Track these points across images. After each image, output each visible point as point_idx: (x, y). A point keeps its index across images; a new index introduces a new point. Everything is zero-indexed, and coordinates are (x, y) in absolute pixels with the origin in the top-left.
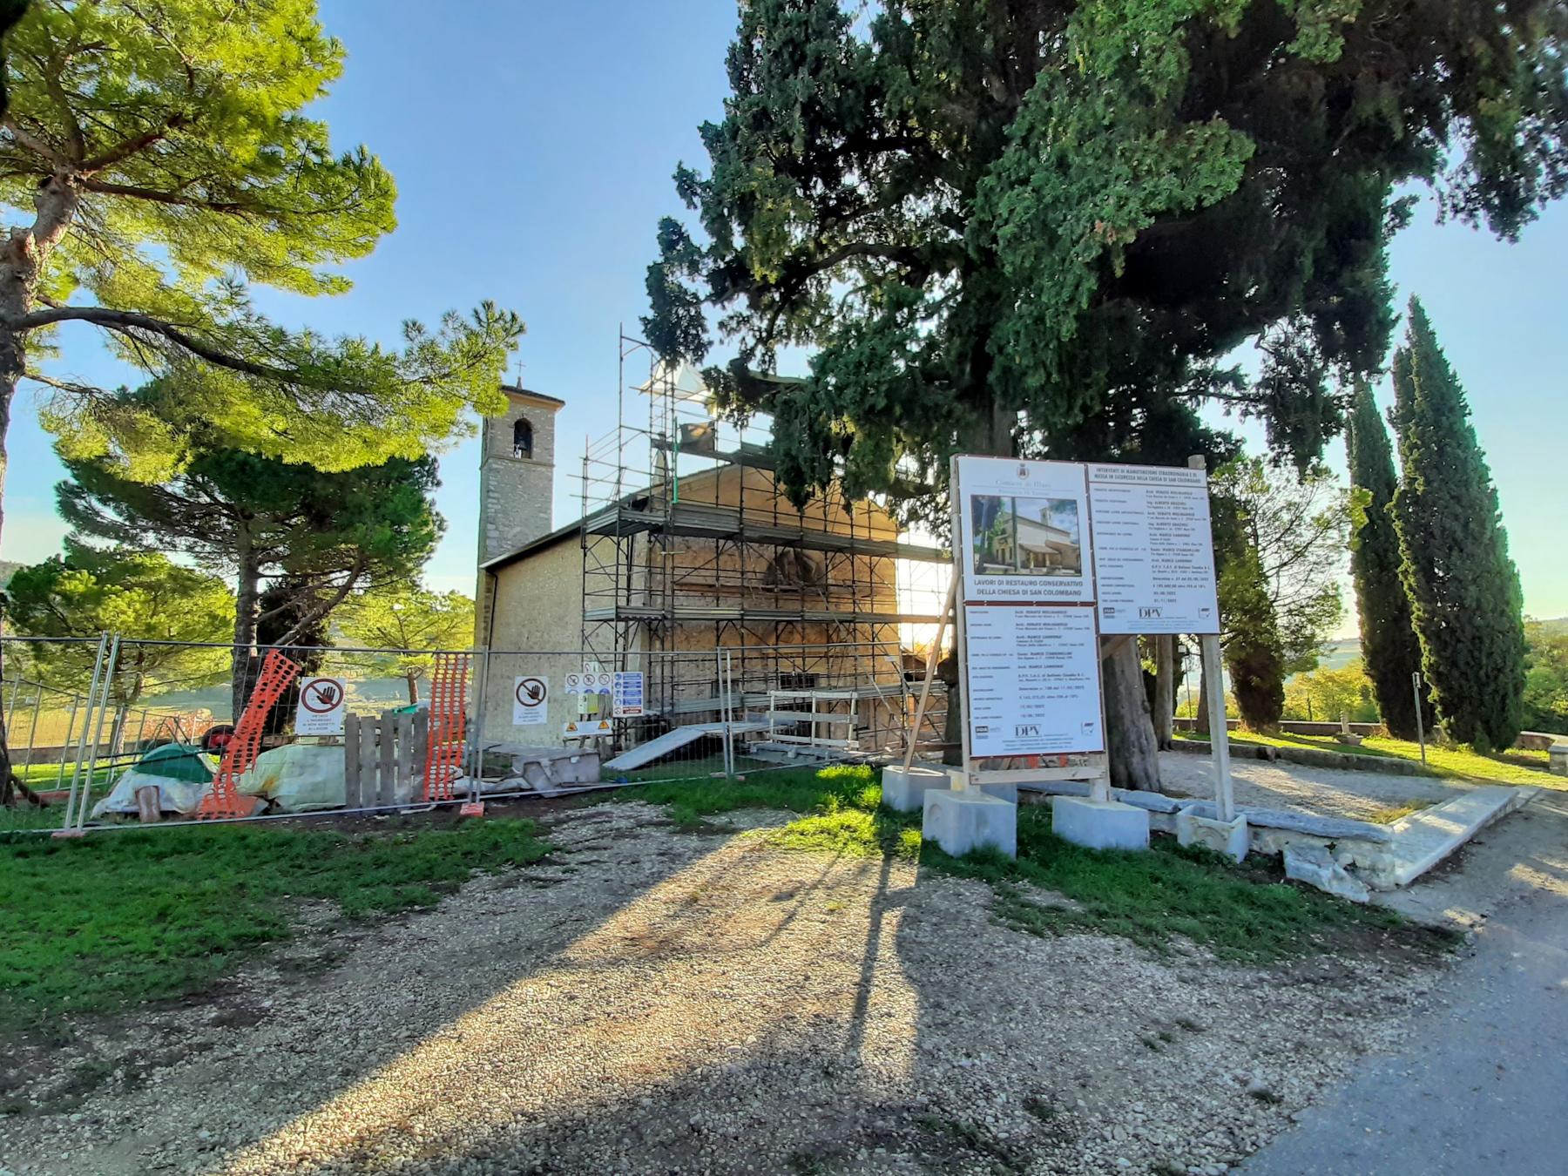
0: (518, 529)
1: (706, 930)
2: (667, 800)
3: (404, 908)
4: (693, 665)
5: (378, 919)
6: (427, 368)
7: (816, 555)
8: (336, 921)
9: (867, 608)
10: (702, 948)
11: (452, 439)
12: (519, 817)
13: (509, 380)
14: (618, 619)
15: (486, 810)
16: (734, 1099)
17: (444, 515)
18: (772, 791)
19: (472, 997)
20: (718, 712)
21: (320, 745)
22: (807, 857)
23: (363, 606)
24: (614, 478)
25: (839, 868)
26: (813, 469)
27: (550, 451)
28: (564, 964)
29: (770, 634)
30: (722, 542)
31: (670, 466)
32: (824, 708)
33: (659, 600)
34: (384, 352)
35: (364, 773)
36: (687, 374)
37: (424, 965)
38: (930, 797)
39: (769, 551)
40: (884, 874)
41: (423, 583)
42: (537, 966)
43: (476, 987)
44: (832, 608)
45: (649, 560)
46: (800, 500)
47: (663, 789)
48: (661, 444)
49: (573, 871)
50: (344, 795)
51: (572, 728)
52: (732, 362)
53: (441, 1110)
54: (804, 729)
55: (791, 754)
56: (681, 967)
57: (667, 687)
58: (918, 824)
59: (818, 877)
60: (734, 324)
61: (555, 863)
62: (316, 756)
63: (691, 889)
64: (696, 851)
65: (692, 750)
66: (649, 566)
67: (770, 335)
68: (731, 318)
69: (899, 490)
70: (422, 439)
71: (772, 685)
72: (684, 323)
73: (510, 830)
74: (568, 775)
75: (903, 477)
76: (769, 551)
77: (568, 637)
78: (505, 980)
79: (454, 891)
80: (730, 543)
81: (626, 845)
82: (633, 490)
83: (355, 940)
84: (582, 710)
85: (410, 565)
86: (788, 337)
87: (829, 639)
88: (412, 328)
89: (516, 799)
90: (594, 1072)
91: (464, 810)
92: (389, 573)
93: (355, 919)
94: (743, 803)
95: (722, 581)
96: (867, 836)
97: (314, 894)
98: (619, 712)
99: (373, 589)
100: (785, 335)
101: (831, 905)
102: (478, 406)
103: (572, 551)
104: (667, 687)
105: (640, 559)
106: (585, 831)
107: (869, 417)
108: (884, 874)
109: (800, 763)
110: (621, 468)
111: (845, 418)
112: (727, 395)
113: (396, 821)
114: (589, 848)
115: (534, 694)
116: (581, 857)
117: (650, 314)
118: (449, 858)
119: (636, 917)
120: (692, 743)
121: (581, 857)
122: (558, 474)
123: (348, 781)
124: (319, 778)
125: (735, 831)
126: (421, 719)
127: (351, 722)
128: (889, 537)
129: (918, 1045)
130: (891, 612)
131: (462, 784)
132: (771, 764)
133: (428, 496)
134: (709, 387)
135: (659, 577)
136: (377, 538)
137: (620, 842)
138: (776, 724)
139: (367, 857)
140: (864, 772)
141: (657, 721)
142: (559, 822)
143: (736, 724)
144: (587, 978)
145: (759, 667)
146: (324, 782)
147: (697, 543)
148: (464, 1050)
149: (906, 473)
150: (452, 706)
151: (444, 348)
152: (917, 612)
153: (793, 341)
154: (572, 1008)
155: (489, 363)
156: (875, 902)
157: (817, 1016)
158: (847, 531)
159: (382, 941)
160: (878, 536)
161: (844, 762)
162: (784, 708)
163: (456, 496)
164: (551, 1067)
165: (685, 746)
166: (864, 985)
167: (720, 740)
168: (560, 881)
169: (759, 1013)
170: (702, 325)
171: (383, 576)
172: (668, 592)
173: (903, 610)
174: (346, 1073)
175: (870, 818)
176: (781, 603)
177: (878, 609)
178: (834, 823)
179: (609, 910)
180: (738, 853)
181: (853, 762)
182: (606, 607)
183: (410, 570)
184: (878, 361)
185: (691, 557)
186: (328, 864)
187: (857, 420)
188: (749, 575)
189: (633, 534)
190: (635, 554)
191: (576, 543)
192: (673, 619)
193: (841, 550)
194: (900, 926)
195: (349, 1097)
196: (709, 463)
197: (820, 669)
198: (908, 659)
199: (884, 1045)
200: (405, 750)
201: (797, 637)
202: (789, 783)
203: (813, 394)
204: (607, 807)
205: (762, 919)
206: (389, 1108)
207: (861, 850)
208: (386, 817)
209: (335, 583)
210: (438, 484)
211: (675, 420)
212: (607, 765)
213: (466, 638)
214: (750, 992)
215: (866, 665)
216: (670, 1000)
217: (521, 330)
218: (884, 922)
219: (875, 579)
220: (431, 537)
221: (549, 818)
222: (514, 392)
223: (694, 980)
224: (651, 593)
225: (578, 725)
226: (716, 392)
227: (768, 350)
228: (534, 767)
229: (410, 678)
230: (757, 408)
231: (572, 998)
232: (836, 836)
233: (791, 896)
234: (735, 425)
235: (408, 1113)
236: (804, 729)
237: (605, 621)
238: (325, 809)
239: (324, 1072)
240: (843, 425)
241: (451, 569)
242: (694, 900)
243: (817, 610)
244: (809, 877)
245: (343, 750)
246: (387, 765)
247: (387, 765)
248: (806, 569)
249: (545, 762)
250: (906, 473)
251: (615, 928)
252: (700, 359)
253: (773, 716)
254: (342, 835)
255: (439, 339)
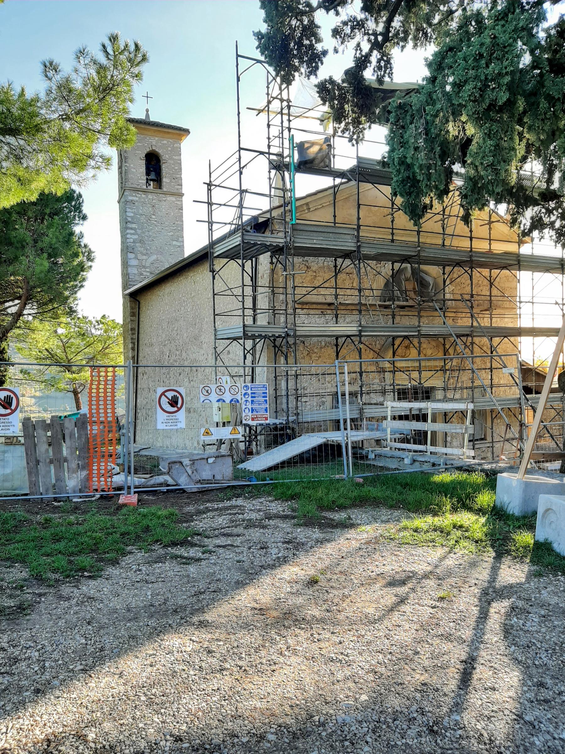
0: (154, 257)
1: (324, 607)
2: (293, 497)
3: (75, 574)
4: (314, 378)
5: (57, 581)
6: (65, 107)
7: (433, 271)
8: (25, 580)
9: (485, 322)
10: (322, 621)
11: (90, 173)
12: (166, 507)
13: (137, 113)
14: (246, 336)
15: (139, 501)
16: (347, 743)
17: (92, 247)
18: (388, 493)
19: (132, 643)
20: (338, 421)
21: (6, 444)
22: (420, 551)
23: (33, 331)
24: (236, 202)
25: (450, 562)
26: (429, 177)
27: (178, 181)
28: (203, 624)
29: (387, 349)
30: (340, 261)
31: (288, 187)
32: (440, 418)
33: (283, 319)
34: (29, 95)
35: (41, 466)
36: (303, 89)
37: (93, 618)
38: (543, 502)
39: (387, 268)
40: (495, 570)
41: (79, 309)
42: (181, 625)
43: (133, 637)
44: (449, 322)
45: (272, 280)
46: (416, 212)
47: (289, 488)
48: (279, 166)
49: (210, 552)
50: (27, 484)
51: (207, 433)
52: (347, 72)
53: (107, 726)
54: (420, 437)
55: (407, 459)
56: (303, 635)
57: (292, 399)
58: (531, 527)
59: (429, 568)
60: (348, 30)
61: (196, 545)
62: (4, 452)
63: (312, 572)
64: (317, 541)
65: (314, 456)
66: (272, 287)
67: (386, 39)
68: (345, 23)
69: (520, 197)
70: (65, 174)
71: (390, 396)
72: (298, 34)
73: (159, 518)
74: (206, 474)
75: (526, 183)
76: (387, 268)
77: (203, 355)
78: (156, 633)
79: (115, 562)
80: (348, 262)
81: (255, 534)
82: (255, 213)
83: (40, 595)
84: (216, 419)
85: (67, 293)
86: (405, 39)
87: (446, 352)
88: (50, 67)
89: (164, 493)
90: (229, 709)
91: (122, 500)
92: (51, 301)
93: (39, 579)
94: (362, 502)
95: (341, 300)
96: (479, 535)
97: (8, 559)
98: (248, 418)
99: (40, 315)
100: (402, 38)
101: (441, 594)
102: (114, 140)
103: (200, 277)
104: (292, 399)
105: (264, 280)
106: (222, 521)
107: (487, 114)
108: (495, 570)
109: (416, 468)
110: (242, 192)
111: (464, 118)
112: (342, 108)
113: (68, 506)
114: (224, 535)
115: (174, 402)
116: (218, 542)
117: (264, 28)
118: (110, 538)
119: (262, 592)
120: (314, 449)
121: (218, 542)
122: (187, 201)
123: (30, 473)
124: (8, 471)
125: (352, 526)
126: (82, 423)
127: (28, 425)
128: (512, 248)
129: (520, 716)
130: (510, 325)
131: (119, 479)
132: (388, 469)
133: (77, 229)
134: (324, 100)
135: (282, 297)
136: (38, 269)
137: (251, 530)
138: (393, 432)
139: (47, 533)
140: (478, 478)
141: (282, 429)
142: (199, 512)
143: (354, 433)
144: (222, 637)
145: (377, 381)
146: (12, 474)
147: (316, 263)
148: (125, 684)
149: (531, 178)
150: (106, 413)
151: (78, 85)
152: (538, 324)
153: (411, 44)
154: (210, 660)
155: (118, 95)
156: (485, 593)
157: (424, 684)
158: (465, 244)
159: (61, 597)
160: (499, 248)
161: (460, 469)
162: (401, 418)
163: (100, 228)
164: (191, 703)
165: (308, 452)
166: (469, 666)
167: (339, 446)
168: (199, 560)
169: (371, 677)
170: (315, 35)
171: (46, 304)
172: (290, 311)
173: (525, 323)
174: (37, 691)
175: (483, 520)
176: (397, 319)
177: (498, 323)
178: (447, 522)
179: (240, 585)
180: (355, 544)
181: (469, 470)
182: (234, 326)
183: (67, 298)
184: (501, 50)
185: (311, 277)
186: (18, 537)
187: (479, 119)
188: (367, 293)
189: (256, 256)
190: (259, 275)
191: (207, 266)
192: (295, 336)
193: (459, 264)
194: (508, 615)
195: (41, 709)
196: (326, 182)
197: (436, 382)
198: (527, 372)
199: (486, 713)
200: (72, 450)
201: (414, 353)
202: (405, 485)
203: (430, 95)
204: (240, 502)
205: (377, 601)
206: (69, 720)
207: (473, 547)
208: (58, 503)
209: (9, 311)
210: (84, 218)
211: (291, 139)
212: (241, 466)
213: (118, 355)
214: (363, 662)
215: (484, 378)
216: (294, 660)
217: (144, 59)
218: (492, 610)
219: (495, 292)
220: (82, 267)
221: (191, 509)
222: (144, 124)
223: (315, 646)
224: (274, 311)
225: (213, 430)
226: (332, 107)
227: (383, 54)
228: (177, 466)
229: (75, 393)
230: (372, 121)
231: (209, 652)
232: (448, 534)
233: (403, 583)
234: (351, 140)
235: (83, 725)
236: (420, 437)
237: (235, 339)
238: (14, 495)
239: (20, 690)
240: (462, 127)
241: (100, 296)
242: (313, 582)
243: (433, 324)
244: (421, 568)
245: (23, 449)
246: (58, 461)
247: (58, 461)
248: (423, 284)
249: (186, 462)
250: (531, 178)
251: (248, 598)
252: (313, 71)
253: (390, 425)
254: (27, 516)
255: (74, 76)
